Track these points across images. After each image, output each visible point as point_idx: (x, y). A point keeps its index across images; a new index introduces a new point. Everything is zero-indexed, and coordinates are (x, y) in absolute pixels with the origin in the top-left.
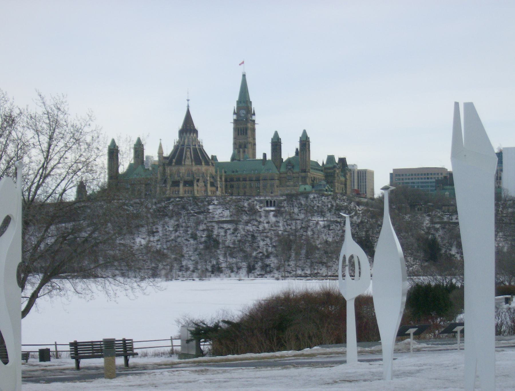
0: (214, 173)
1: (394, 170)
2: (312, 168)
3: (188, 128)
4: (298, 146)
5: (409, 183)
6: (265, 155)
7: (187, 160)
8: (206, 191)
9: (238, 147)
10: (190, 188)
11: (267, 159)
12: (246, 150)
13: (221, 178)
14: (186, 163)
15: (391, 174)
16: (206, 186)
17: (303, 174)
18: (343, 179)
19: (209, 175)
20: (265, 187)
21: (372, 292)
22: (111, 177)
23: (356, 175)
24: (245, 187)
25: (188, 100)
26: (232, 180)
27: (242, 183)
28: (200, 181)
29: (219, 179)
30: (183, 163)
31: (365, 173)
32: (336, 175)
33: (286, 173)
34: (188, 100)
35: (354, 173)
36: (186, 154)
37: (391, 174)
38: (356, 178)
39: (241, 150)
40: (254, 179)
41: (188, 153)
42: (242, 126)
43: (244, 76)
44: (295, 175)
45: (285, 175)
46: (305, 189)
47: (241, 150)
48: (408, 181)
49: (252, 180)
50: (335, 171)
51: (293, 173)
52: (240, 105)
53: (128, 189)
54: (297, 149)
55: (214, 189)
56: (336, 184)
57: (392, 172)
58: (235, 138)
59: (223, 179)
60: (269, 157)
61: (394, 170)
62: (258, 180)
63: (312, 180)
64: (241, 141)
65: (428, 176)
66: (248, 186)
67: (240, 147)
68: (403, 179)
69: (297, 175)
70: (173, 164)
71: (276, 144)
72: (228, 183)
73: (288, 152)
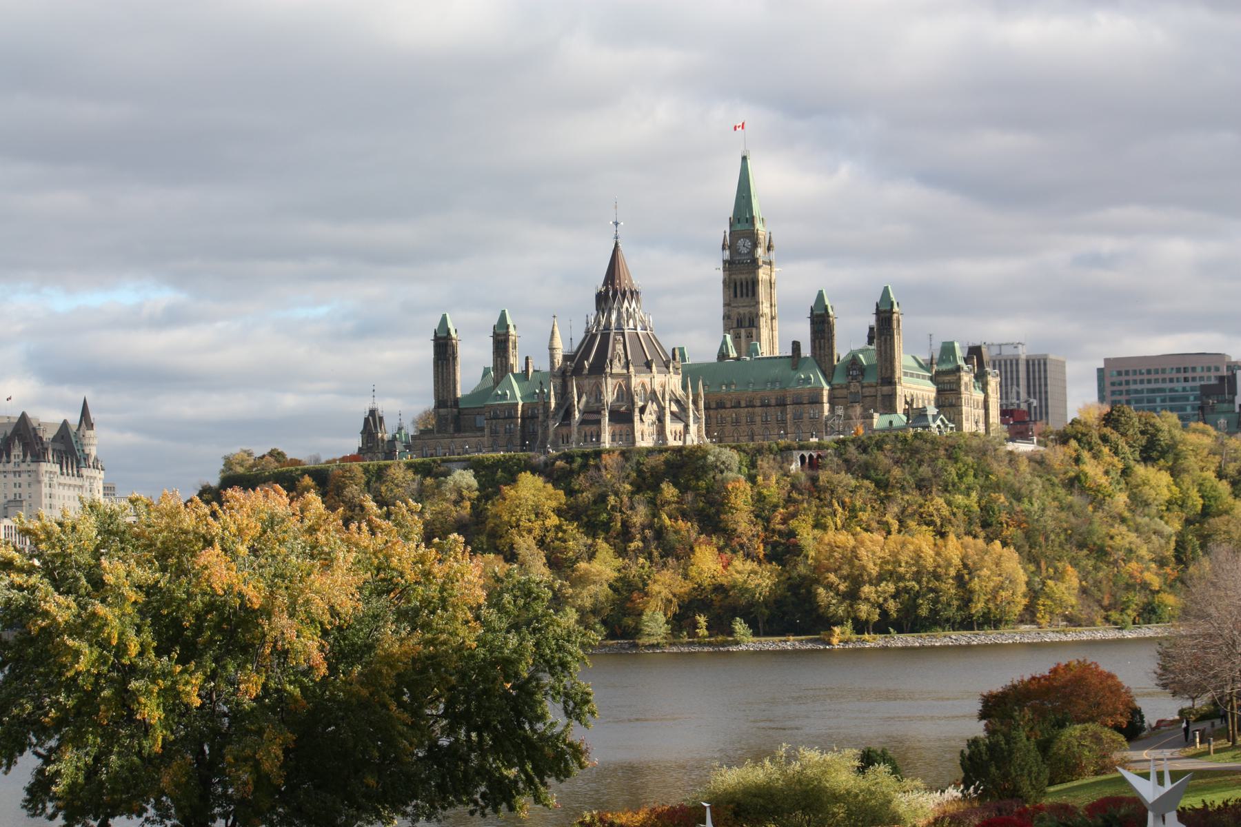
0: (679, 392)
1: (1107, 361)
2: (906, 374)
3: (612, 291)
4: (872, 321)
5: (1142, 391)
6: (796, 346)
7: (616, 362)
8: (661, 432)
9: (735, 325)
10: (625, 427)
11: (803, 355)
12: (754, 331)
13: (695, 402)
14: (614, 371)
15: (1100, 371)
16: (660, 420)
17: (886, 389)
18: (979, 396)
19: (667, 397)
20: (798, 417)
21: (856, 751)
22: (440, 403)
23: (1022, 368)
24: (753, 422)
25: (616, 224)
26: (721, 405)
27: (744, 411)
28: (647, 411)
29: (691, 406)
30: (608, 370)
31: (1045, 364)
32: (963, 388)
33: (847, 387)
34: (616, 224)
35: (1017, 364)
36: (614, 349)
37: (1100, 371)
38: (1022, 374)
39: (743, 331)
40: (773, 402)
41: (620, 347)
42: (743, 277)
43: (744, 159)
44: (867, 391)
45: (845, 392)
46: (891, 422)
47: (743, 331)
48: (1139, 387)
49: (769, 405)
50: (959, 379)
51: (863, 387)
52: (738, 227)
53: (482, 429)
54: (871, 329)
55: (680, 427)
56: (964, 408)
57: (1102, 365)
58: (726, 305)
59: (702, 404)
60: (806, 351)
61: (1107, 361)
62: (782, 404)
63: (906, 403)
64: (741, 311)
65: (1187, 375)
66: (758, 419)
67: (740, 324)
68: (1127, 383)
69: (871, 391)
70: (586, 372)
71: (821, 322)
72: (712, 412)
73: (851, 336)
